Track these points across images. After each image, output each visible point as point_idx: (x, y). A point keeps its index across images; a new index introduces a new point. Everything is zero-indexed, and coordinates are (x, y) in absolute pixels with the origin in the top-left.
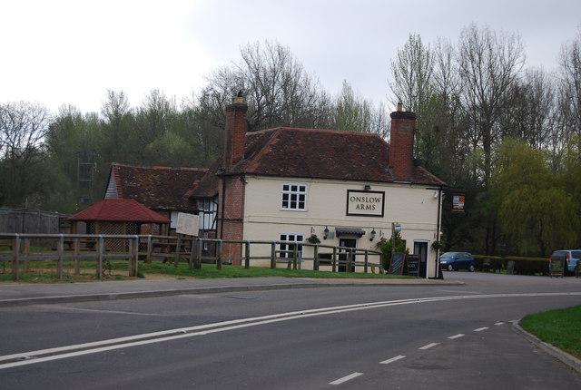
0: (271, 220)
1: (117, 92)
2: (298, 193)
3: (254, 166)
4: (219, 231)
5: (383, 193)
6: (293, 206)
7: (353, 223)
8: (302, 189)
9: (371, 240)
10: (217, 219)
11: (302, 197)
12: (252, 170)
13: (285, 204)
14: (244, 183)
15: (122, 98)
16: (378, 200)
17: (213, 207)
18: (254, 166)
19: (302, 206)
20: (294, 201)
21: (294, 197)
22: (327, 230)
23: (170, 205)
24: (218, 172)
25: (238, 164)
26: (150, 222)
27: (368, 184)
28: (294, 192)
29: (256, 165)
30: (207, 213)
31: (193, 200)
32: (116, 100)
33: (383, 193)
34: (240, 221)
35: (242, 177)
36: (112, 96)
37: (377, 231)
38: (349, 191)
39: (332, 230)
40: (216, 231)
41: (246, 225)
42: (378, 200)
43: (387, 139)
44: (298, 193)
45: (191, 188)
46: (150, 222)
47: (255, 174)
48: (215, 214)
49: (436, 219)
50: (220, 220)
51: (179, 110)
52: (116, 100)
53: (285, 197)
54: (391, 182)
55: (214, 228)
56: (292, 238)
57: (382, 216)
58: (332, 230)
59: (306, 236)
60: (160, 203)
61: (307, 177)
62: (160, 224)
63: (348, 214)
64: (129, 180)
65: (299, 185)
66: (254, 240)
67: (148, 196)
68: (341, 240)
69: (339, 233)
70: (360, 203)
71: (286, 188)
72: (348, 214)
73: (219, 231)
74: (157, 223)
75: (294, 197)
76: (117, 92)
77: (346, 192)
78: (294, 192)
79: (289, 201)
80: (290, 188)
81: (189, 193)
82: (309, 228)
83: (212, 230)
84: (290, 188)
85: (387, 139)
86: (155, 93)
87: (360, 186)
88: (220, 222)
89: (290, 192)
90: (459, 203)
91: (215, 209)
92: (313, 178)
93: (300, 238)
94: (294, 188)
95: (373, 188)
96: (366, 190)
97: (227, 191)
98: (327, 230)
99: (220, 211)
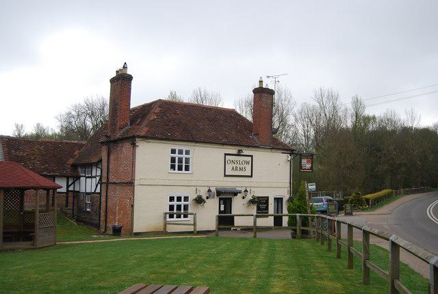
0: (274, 185)
1: (20, 124)
2: (182, 203)
3: (144, 131)
4: (104, 194)
5: (252, 156)
6: (180, 168)
7: (229, 184)
8: (188, 152)
9: (243, 198)
10: (100, 182)
11: (187, 160)
12: (143, 134)
13: (173, 167)
14: (134, 145)
15: (22, 127)
16: (248, 163)
17: (96, 172)
18: (144, 131)
19: (187, 168)
20: (180, 165)
21: (180, 160)
22: (209, 191)
23: (54, 171)
24: (103, 139)
25: (124, 130)
26: (36, 189)
27: (240, 148)
28: (180, 156)
29: (146, 129)
30: (89, 177)
31: (75, 167)
32: (19, 128)
33: (252, 156)
34: (131, 184)
35: (132, 140)
36: (17, 126)
37: (248, 189)
38: (226, 154)
39: (213, 190)
40: (100, 193)
41: (137, 188)
42: (248, 163)
43: (250, 118)
44: (182, 203)
45: (72, 157)
46: (36, 189)
47: (145, 138)
48: (98, 178)
49: (289, 178)
50: (105, 183)
51: (50, 133)
52: (19, 128)
53: (173, 160)
54: (258, 147)
55: (98, 190)
56: (179, 199)
57: (251, 176)
58: (213, 190)
59: (192, 196)
60: (45, 169)
61: (192, 141)
62: (47, 189)
63: (225, 176)
64: (16, 150)
65: (184, 148)
66: (238, 213)
67: (34, 164)
68: (220, 199)
69: (219, 193)
70: (235, 166)
71: (173, 151)
72: (225, 176)
73: (104, 194)
74: (44, 189)
75: (180, 160)
76: (20, 124)
77: (224, 155)
78: (180, 156)
79: (177, 164)
80: (177, 152)
81: (71, 161)
82: (194, 188)
83: (95, 193)
84: (177, 152)
85: (250, 118)
86: (38, 125)
87: (234, 150)
88: (104, 186)
89: (175, 203)
90: (306, 164)
91: (99, 173)
92: (197, 142)
93: (186, 199)
94: (181, 152)
95: (246, 152)
96: (238, 155)
97: (112, 157)
98: (209, 191)
99: (105, 175)
